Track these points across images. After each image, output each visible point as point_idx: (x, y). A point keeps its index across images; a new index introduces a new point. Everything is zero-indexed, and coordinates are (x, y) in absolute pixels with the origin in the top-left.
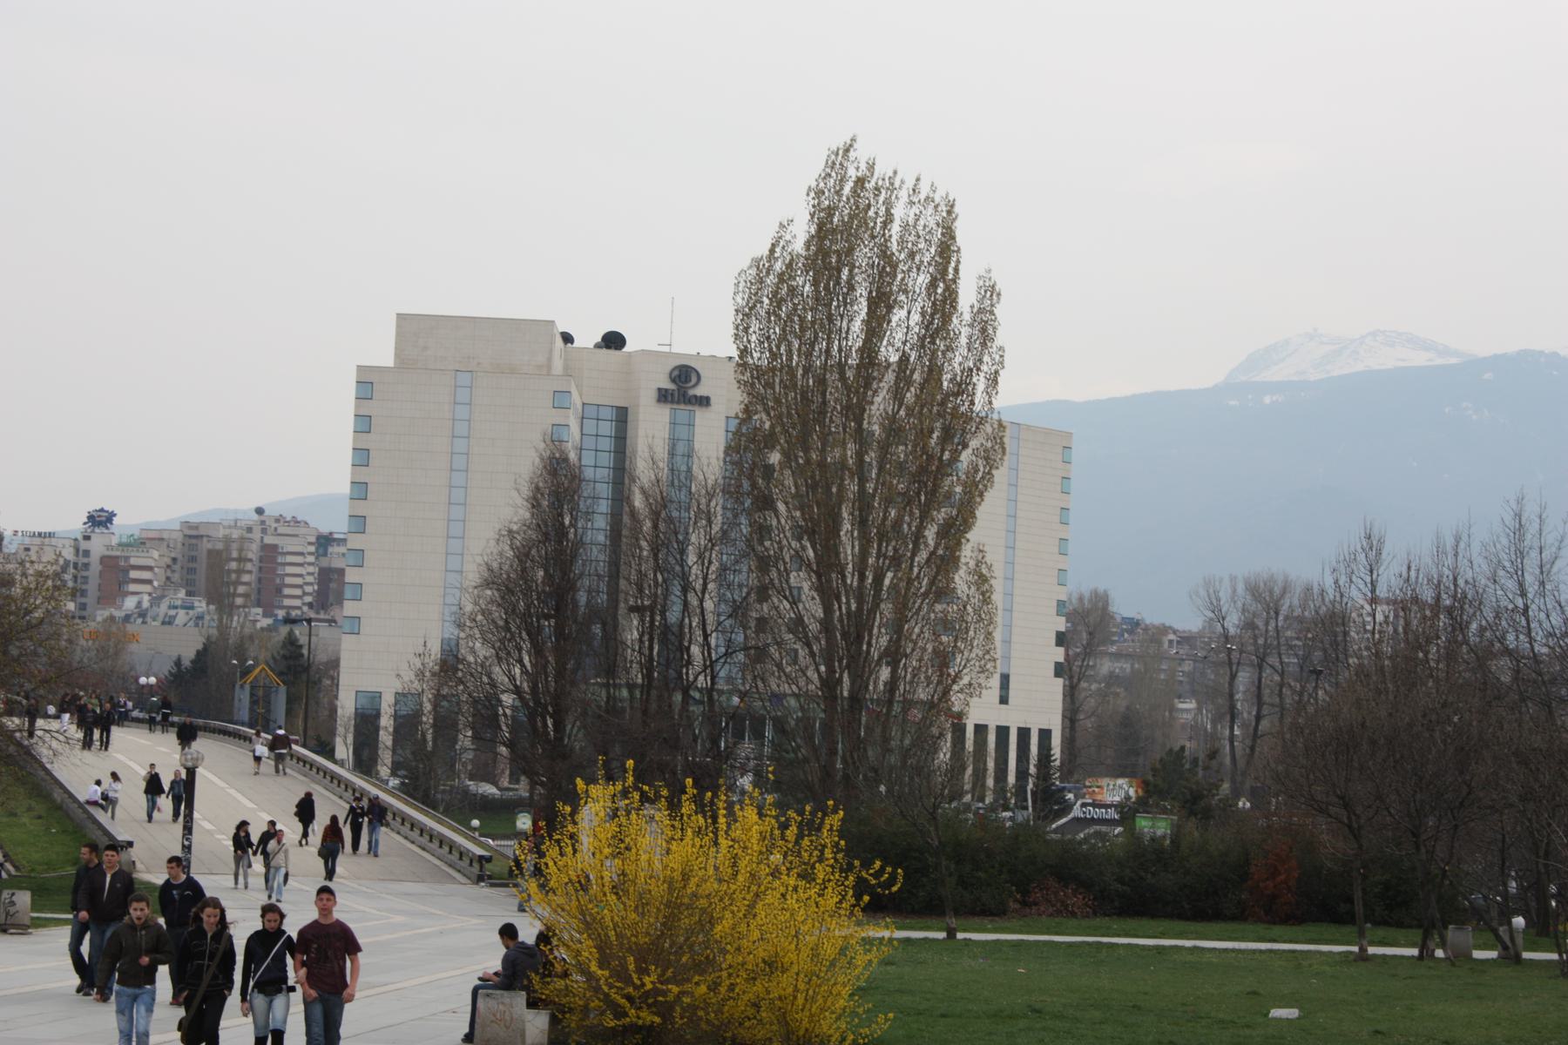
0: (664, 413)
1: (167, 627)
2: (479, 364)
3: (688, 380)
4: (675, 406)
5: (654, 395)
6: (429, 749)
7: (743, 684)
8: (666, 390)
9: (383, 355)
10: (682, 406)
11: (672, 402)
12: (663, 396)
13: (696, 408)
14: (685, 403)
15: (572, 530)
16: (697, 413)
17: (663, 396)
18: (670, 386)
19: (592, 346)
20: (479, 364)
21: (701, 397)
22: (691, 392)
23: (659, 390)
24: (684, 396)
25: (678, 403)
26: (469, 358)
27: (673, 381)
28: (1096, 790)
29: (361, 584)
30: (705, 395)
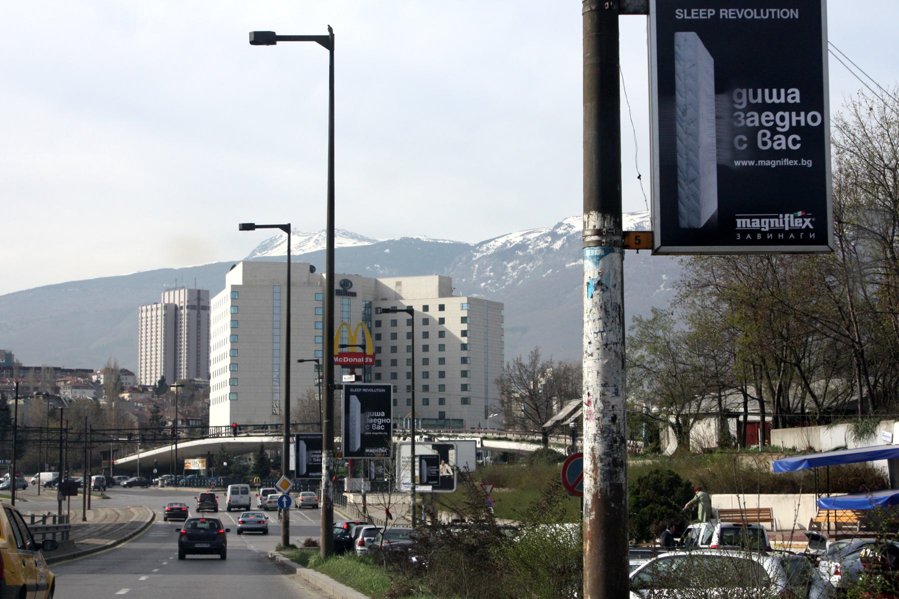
4: (343, 297)
8: (339, 290)
11: (341, 295)
25: (344, 295)
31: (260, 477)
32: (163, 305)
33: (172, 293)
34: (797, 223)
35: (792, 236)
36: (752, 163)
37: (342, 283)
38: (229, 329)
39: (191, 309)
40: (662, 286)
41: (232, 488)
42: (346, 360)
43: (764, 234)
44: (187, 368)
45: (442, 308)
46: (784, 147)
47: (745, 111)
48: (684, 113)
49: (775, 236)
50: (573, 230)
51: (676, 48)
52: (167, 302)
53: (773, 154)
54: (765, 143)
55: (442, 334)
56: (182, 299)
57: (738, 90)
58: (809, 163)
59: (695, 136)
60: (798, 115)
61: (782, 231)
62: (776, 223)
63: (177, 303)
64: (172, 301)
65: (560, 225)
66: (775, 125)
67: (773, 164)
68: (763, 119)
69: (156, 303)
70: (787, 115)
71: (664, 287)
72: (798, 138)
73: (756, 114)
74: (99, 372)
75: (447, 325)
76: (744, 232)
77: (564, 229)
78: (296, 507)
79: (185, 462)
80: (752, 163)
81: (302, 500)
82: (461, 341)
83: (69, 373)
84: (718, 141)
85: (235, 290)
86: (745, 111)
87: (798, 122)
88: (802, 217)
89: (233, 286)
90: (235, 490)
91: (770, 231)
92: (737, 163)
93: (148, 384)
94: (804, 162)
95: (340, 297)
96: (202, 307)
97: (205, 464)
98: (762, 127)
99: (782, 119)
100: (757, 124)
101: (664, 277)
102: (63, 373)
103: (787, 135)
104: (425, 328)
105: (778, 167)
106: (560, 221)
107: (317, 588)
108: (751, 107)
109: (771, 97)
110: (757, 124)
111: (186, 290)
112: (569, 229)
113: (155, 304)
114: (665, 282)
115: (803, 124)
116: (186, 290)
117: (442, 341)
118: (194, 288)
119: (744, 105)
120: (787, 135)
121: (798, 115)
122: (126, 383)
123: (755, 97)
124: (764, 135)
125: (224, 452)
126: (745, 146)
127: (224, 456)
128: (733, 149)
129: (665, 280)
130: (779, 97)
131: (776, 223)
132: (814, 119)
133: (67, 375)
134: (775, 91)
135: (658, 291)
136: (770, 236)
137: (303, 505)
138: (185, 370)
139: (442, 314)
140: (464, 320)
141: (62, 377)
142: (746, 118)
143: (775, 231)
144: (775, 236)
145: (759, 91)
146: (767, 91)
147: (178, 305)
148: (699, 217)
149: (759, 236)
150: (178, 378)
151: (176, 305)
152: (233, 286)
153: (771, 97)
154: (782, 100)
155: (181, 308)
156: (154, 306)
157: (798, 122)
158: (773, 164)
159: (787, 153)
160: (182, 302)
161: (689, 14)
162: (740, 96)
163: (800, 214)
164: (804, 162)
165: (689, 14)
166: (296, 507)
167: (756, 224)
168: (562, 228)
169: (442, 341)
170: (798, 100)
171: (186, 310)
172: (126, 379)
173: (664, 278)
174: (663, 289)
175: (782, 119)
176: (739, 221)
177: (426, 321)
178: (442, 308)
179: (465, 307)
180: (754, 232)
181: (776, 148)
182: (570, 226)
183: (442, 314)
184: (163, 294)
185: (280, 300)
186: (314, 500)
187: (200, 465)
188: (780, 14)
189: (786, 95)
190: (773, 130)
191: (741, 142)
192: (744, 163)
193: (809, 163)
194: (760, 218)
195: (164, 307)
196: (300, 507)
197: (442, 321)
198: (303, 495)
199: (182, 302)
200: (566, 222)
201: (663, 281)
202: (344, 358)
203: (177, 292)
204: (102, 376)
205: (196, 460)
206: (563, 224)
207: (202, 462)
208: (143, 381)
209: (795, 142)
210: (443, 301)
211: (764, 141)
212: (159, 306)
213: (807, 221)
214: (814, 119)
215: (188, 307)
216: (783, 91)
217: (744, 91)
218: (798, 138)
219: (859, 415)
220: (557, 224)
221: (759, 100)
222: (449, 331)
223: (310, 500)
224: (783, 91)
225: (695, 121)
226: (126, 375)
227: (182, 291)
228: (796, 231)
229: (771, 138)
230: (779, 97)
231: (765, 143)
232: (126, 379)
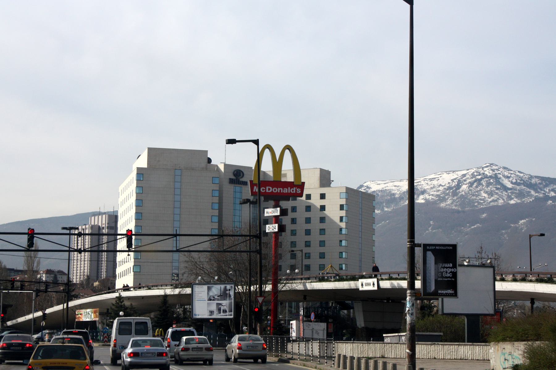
0: (232, 187)
1: (340, 263)
2: (180, 167)
3: (240, 175)
4: (235, 185)
5: (228, 181)
6: (254, 327)
7: (271, 255)
8: (232, 179)
9: (143, 162)
10: (238, 185)
11: (234, 183)
12: (231, 181)
13: (242, 186)
14: (239, 184)
15: (512, 179)
16: (243, 188)
17: (231, 181)
18: (233, 177)
19: (208, 157)
20: (180, 167)
21: (244, 182)
22: (241, 180)
23: (230, 179)
24: (238, 181)
25: (236, 184)
26: (176, 165)
27: (234, 175)
28: (80, 316)
29: (310, 253)
30: (246, 181)
31: (163, 329)
32: (90, 226)
33: (100, 217)
34: (451, 292)
35: (450, 295)
36: (442, 279)
37: (235, 172)
38: (134, 221)
39: (110, 229)
40: (430, 229)
41: (120, 324)
42: (269, 189)
43: (444, 294)
44: (106, 272)
45: (323, 196)
46: (448, 276)
47: (441, 268)
48: (428, 268)
49: (446, 294)
50: (370, 190)
51: (427, 255)
52: (93, 224)
53: (446, 277)
54: (445, 275)
55: (323, 220)
56: (104, 222)
57: (439, 264)
58: (454, 279)
59: (430, 273)
60: (452, 269)
61: (448, 293)
62: (446, 292)
63: (100, 224)
64: (96, 223)
65: (361, 186)
66: (447, 271)
67: (446, 279)
68: (444, 270)
69: (86, 225)
70: (449, 269)
71: (431, 229)
72: (451, 274)
73: (443, 269)
74: (42, 272)
75: (328, 212)
76: (440, 293)
77: (364, 190)
78: (228, 359)
79: (77, 313)
80: (442, 279)
81: (239, 348)
82: (339, 226)
83: (20, 273)
84: (435, 274)
85: (140, 172)
86: (441, 268)
87: (452, 271)
88: (452, 291)
89: (139, 169)
90: (123, 327)
91: (445, 294)
92: (439, 279)
93: (78, 282)
94: (452, 279)
95: (233, 185)
96: (113, 229)
97: (98, 314)
98: (444, 272)
99: (448, 270)
100: (443, 271)
101: (431, 222)
102: (16, 273)
103: (449, 273)
104: (308, 215)
105: (447, 280)
106: (361, 184)
107: (452, 316)
108: (442, 267)
109: (446, 265)
110: (443, 271)
111: (107, 215)
112: (367, 189)
113: (84, 225)
114: (432, 226)
115: (452, 271)
116: (107, 215)
117: (322, 226)
118: (113, 214)
119: (440, 267)
120: (449, 273)
121: (452, 269)
122: (61, 280)
123: (443, 265)
124: (444, 273)
125: (121, 302)
126: (440, 276)
127: (121, 306)
128: (438, 276)
129: (432, 225)
130: (448, 265)
131: (446, 292)
132: (455, 270)
133: (18, 274)
134: (447, 264)
135: (427, 232)
136: (445, 294)
137: (241, 356)
138: (105, 273)
139: (323, 202)
140: (342, 207)
141: (15, 276)
142: (441, 270)
143: (446, 294)
144: (446, 294)
145: (444, 264)
146: (445, 264)
147: (101, 226)
148: (431, 290)
149: (443, 294)
150: (100, 279)
151: (99, 226)
152: (139, 169)
153: (446, 265)
154: (448, 266)
155: (103, 228)
156: (84, 227)
157: (452, 271)
158: (446, 279)
159: (449, 277)
160: (104, 224)
161: (430, 248)
162: (440, 265)
163: (451, 290)
164: (452, 279)
165: (430, 248)
166: (228, 359)
167: (442, 292)
168: (363, 189)
169: (322, 226)
170: (451, 266)
171: (106, 230)
172: (61, 277)
173: (431, 224)
174: (431, 231)
175: (448, 270)
176: (439, 291)
177: (308, 208)
178: (323, 196)
179: (344, 195)
180: (442, 294)
181: (447, 276)
182: (368, 187)
183: (323, 202)
184: (90, 218)
185: (174, 214)
186: (260, 348)
187: (93, 317)
188: (448, 248)
189: (449, 265)
190: (446, 272)
191: (440, 275)
192: (440, 279)
193: (454, 279)
194: (443, 291)
195: (91, 227)
196: (236, 361)
197: (323, 208)
198: (240, 339)
199: (104, 224)
200: (365, 185)
201: (431, 225)
202: (267, 188)
203: (100, 217)
204: (44, 275)
205: (88, 310)
206: (364, 186)
207: (95, 312)
208: (74, 280)
209: (451, 275)
210: (324, 190)
211: (444, 274)
212: (87, 226)
213: (453, 292)
214: (455, 270)
215: (108, 228)
216: (448, 264)
217: (441, 264)
218: (451, 274)
219: (228, 299)
220: (359, 186)
221: (444, 266)
222: (328, 217)
223: (254, 347)
224: (448, 264)
225: (430, 270)
226: (61, 275)
227: (104, 216)
228: (451, 294)
229: (446, 274)
230: (448, 265)
231: (445, 275)
232: (61, 277)
